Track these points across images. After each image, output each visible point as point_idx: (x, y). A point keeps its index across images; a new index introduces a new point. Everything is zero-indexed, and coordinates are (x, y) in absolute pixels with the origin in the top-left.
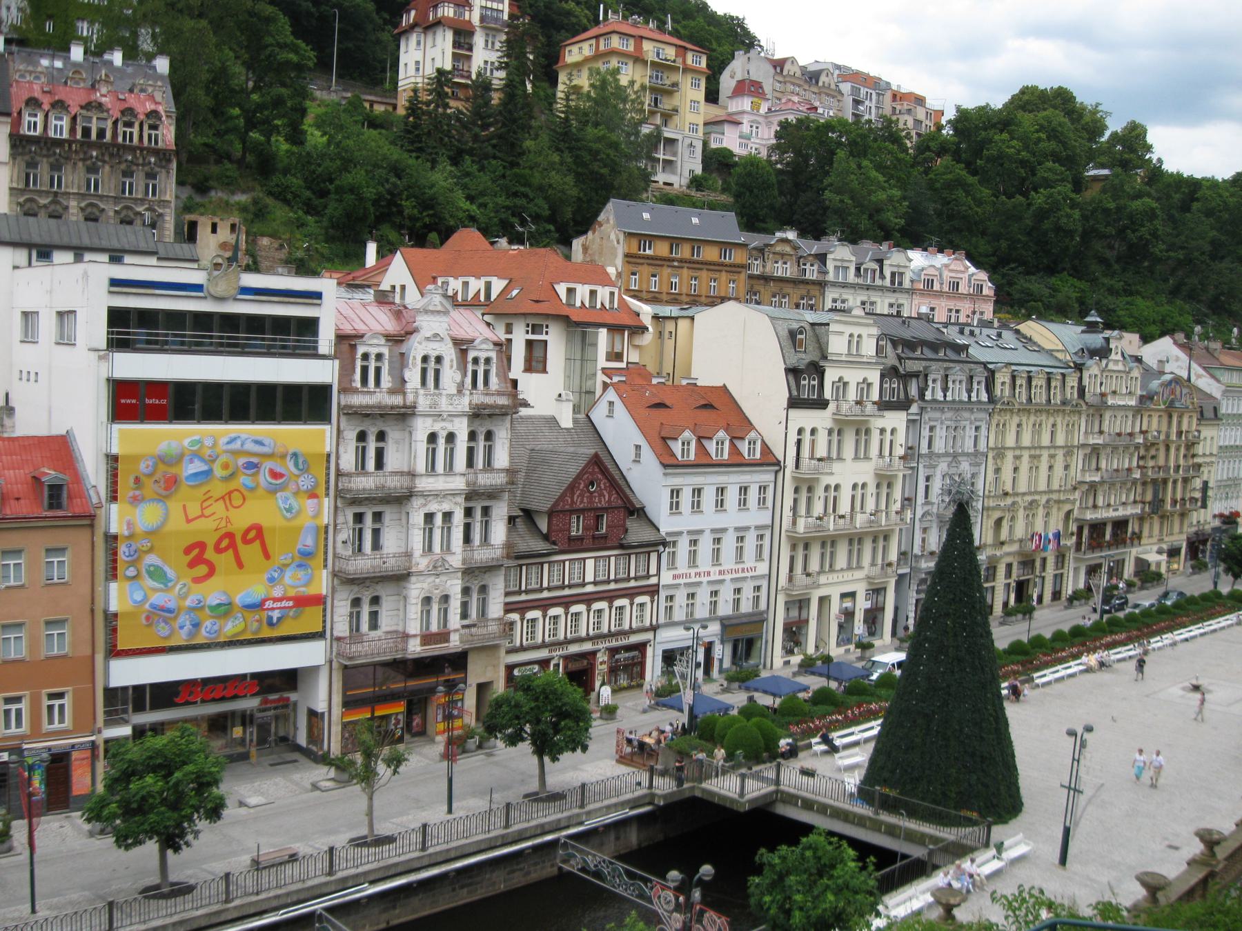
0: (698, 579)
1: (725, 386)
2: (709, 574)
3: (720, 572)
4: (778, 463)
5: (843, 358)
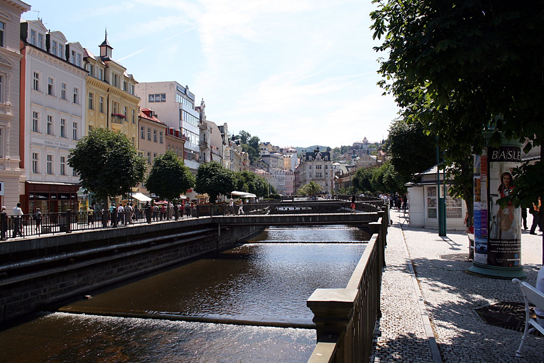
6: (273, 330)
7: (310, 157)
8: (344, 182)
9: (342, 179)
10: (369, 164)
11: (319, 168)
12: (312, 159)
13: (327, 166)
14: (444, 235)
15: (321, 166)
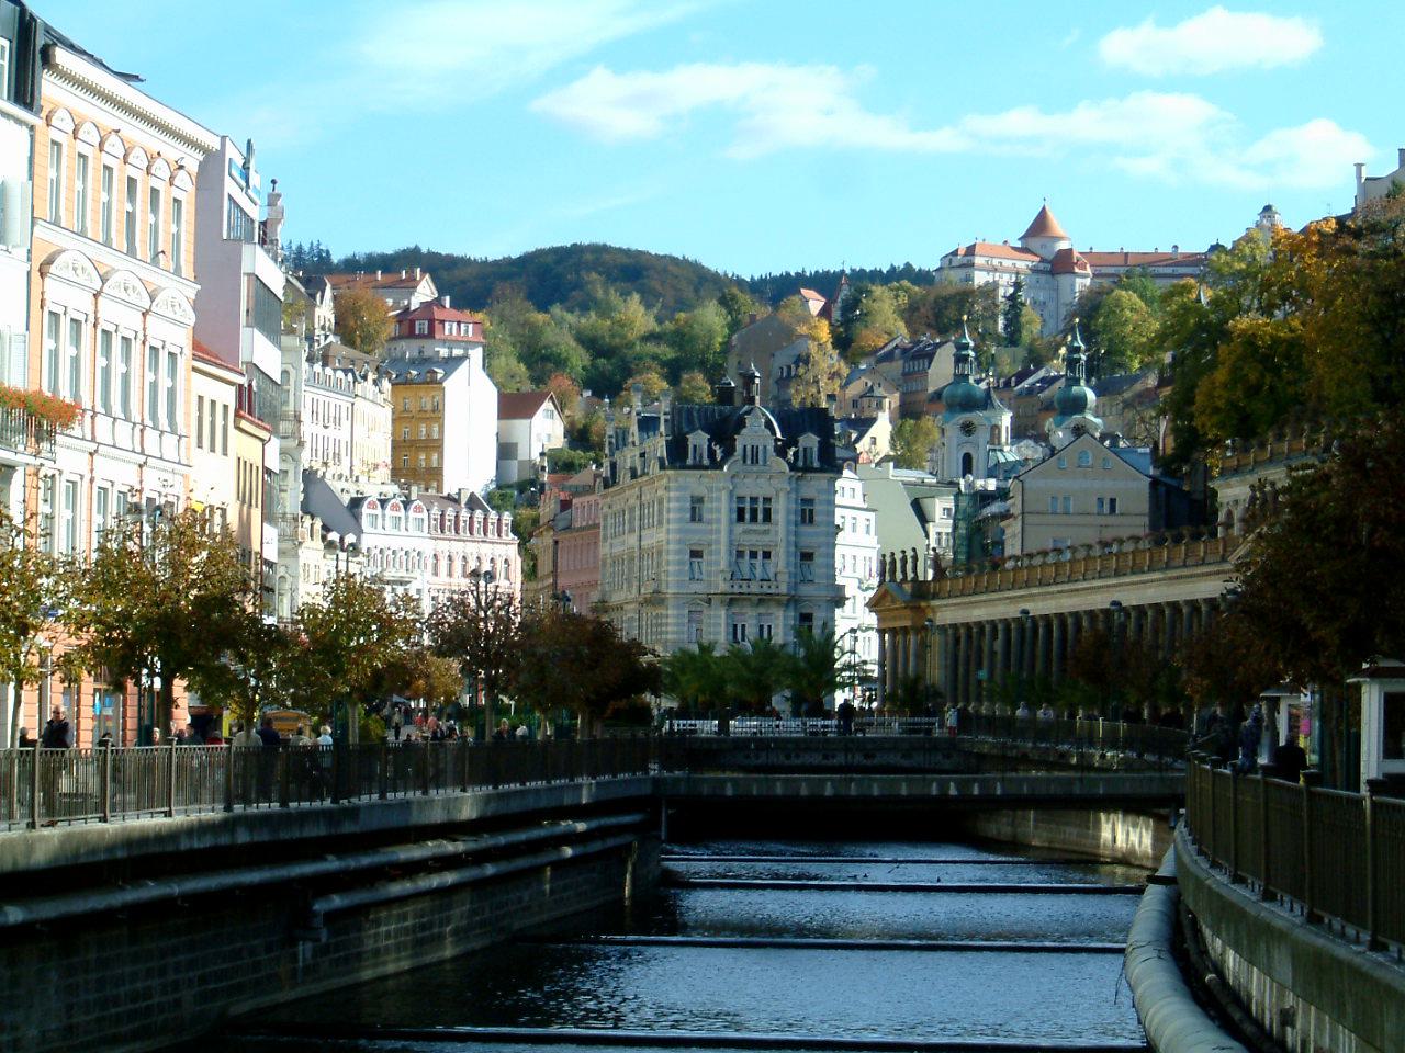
6: (792, 569)
7: (699, 439)
8: (943, 628)
9: (934, 610)
10: (1101, 501)
11: (754, 519)
12: (712, 454)
13: (810, 501)
14: (834, 530)
15: (767, 500)
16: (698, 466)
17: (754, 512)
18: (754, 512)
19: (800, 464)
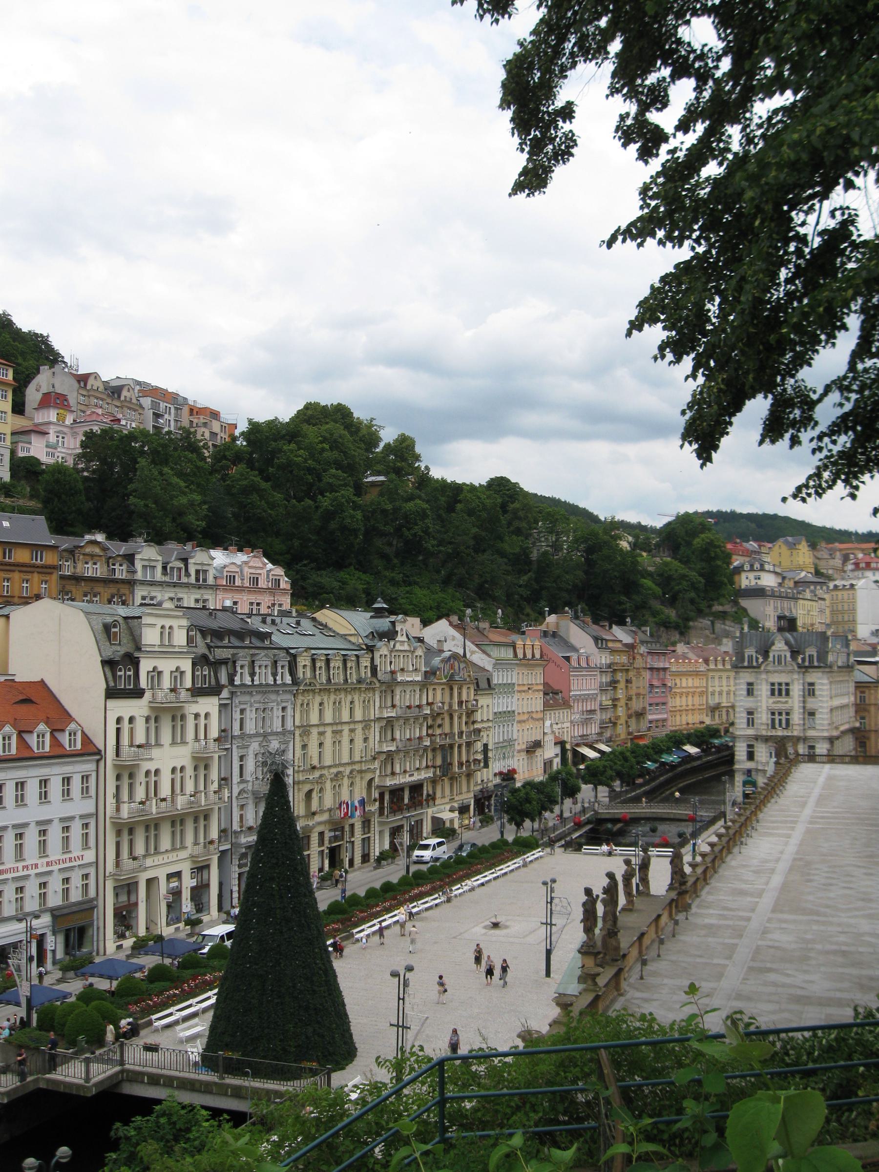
0: (26, 873)
1: (42, 681)
2: (36, 866)
3: (48, 864)
4: (99, 752)
5: (157, 649)
15: (787, 684)
16: (750, 667)
17: (780, 690)
18: (780, 690)
19: (807, 664)
